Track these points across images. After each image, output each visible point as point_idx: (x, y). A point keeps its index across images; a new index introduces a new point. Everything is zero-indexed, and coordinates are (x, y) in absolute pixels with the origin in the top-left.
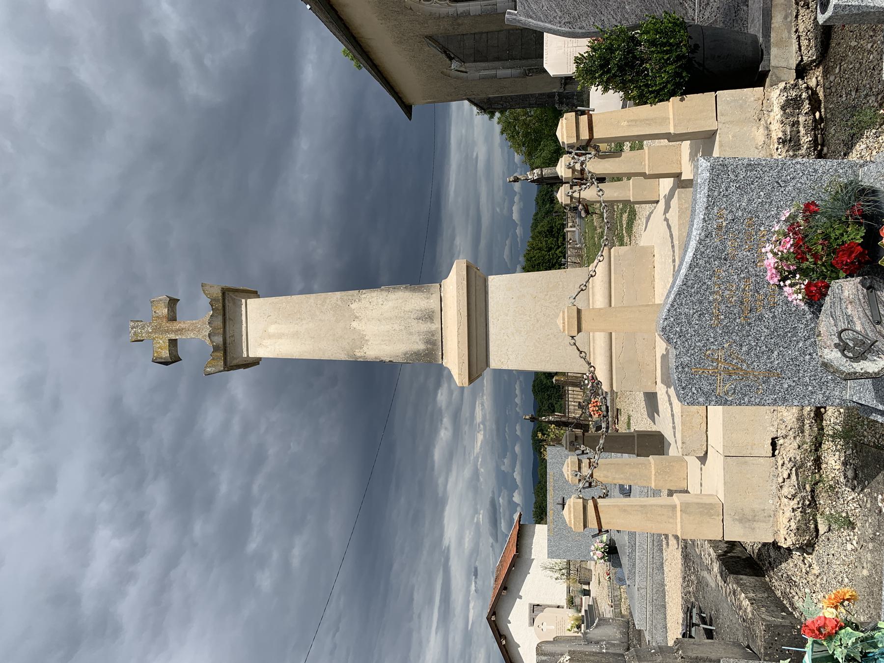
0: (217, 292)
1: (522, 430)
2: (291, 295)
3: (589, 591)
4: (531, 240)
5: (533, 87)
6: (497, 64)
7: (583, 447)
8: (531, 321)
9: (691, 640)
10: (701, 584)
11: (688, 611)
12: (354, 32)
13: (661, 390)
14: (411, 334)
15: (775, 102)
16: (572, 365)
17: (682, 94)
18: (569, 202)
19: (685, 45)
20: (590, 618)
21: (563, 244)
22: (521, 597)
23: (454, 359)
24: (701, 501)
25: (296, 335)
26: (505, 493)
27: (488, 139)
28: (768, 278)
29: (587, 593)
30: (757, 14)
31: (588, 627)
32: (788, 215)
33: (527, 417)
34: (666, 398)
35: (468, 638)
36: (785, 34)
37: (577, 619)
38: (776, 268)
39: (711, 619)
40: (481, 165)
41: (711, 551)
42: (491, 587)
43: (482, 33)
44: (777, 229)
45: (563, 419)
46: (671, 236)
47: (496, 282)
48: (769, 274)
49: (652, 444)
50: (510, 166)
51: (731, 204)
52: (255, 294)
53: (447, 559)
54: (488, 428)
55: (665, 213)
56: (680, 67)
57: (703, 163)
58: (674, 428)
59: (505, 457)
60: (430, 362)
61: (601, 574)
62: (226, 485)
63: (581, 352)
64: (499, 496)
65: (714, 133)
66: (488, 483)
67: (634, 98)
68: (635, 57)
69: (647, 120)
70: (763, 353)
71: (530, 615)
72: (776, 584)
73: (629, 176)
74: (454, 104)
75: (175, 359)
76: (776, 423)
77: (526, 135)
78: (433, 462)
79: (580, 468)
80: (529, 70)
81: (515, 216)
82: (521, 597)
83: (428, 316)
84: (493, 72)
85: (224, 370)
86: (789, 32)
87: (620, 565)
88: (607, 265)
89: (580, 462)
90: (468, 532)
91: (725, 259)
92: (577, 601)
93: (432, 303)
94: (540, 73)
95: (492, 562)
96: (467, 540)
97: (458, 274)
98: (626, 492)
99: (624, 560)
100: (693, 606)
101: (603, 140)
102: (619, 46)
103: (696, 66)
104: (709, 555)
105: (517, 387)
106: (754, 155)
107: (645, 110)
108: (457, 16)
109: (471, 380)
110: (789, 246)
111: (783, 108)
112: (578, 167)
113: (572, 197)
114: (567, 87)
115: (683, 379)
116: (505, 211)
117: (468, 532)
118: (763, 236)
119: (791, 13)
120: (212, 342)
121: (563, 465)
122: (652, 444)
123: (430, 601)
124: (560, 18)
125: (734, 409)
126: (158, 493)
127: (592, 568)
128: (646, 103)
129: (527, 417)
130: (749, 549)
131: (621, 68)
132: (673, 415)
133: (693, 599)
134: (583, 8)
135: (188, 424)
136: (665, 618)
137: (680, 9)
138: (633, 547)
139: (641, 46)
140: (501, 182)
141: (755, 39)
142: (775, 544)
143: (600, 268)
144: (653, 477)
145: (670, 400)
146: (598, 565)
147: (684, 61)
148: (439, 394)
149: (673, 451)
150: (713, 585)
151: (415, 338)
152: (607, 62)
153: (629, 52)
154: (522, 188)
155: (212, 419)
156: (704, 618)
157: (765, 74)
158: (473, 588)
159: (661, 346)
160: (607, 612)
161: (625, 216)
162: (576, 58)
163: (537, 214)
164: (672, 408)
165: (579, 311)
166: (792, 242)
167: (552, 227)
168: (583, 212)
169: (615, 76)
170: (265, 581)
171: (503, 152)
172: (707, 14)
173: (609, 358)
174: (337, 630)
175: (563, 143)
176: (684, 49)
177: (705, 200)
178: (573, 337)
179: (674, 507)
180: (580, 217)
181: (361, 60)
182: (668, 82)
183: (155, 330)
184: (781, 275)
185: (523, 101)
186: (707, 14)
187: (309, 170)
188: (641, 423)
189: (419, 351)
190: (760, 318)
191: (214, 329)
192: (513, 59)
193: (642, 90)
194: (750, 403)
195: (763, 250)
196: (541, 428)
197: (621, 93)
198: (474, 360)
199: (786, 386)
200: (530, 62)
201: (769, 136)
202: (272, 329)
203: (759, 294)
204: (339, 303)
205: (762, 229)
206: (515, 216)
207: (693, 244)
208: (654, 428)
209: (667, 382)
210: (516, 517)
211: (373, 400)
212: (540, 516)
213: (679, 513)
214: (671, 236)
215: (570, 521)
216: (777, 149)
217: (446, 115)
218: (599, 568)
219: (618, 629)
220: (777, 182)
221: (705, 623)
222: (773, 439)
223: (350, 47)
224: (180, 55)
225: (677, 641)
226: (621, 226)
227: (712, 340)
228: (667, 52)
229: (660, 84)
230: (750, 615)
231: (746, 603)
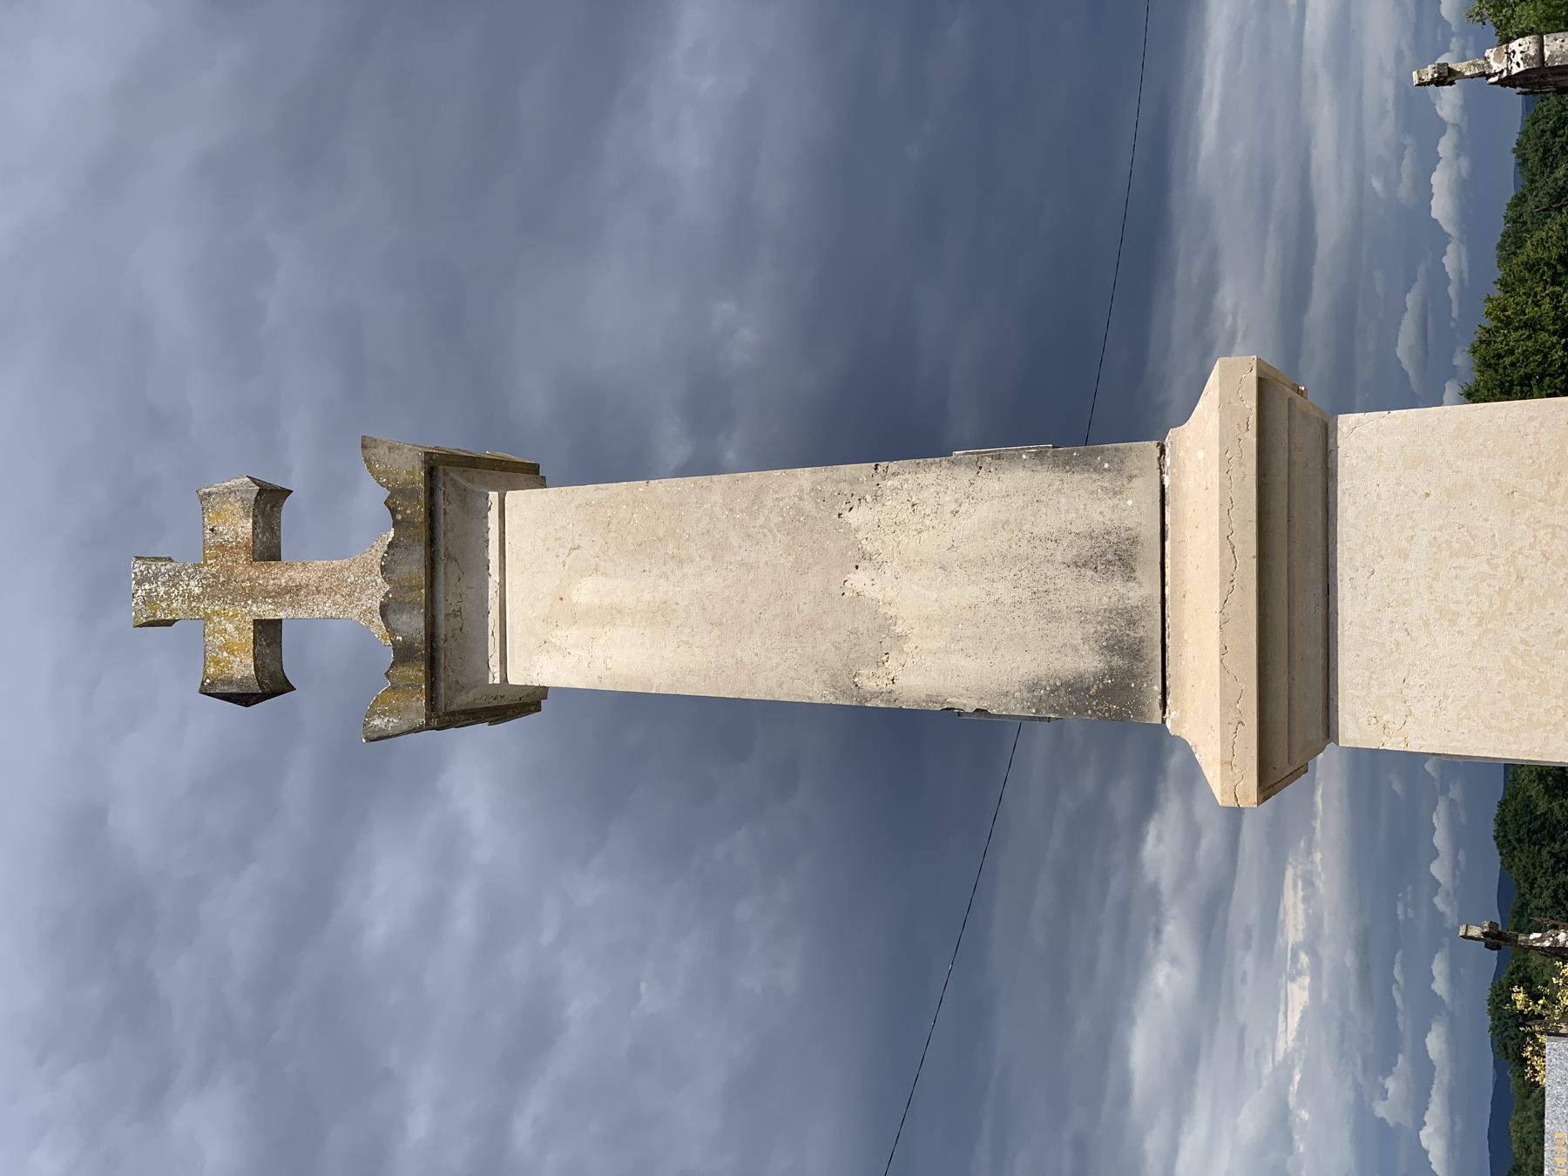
0: (410, 468)
1: (1453, 978)
4: (1497, 293)
14: (1054, 616)
25: (660, 614)
33: (1475, 931)
47: (1369, 442)
52: (530, 474)
54: (1326, 966)
59: (1387, 1070)
60: (1119, 717)
75: (270, 684)
81: (1441, 207)
83: (1115, 556)
85: (427, 727)
97: (1224, 405)
105: (1439, 820)
109: (1268, 784)
116: (1404, 190)
120: (392, 631)
129: (1475, 931)
140: (1389, 88)
148: (1151, 839)
151: (1072, 632)
155: (387, 888)
163: (1520, 200)
183: (214, 589)
191: (399, 587)
202: (585, 592)
204: (808, 505)
206: (1441, 207)
211: (928, 847)
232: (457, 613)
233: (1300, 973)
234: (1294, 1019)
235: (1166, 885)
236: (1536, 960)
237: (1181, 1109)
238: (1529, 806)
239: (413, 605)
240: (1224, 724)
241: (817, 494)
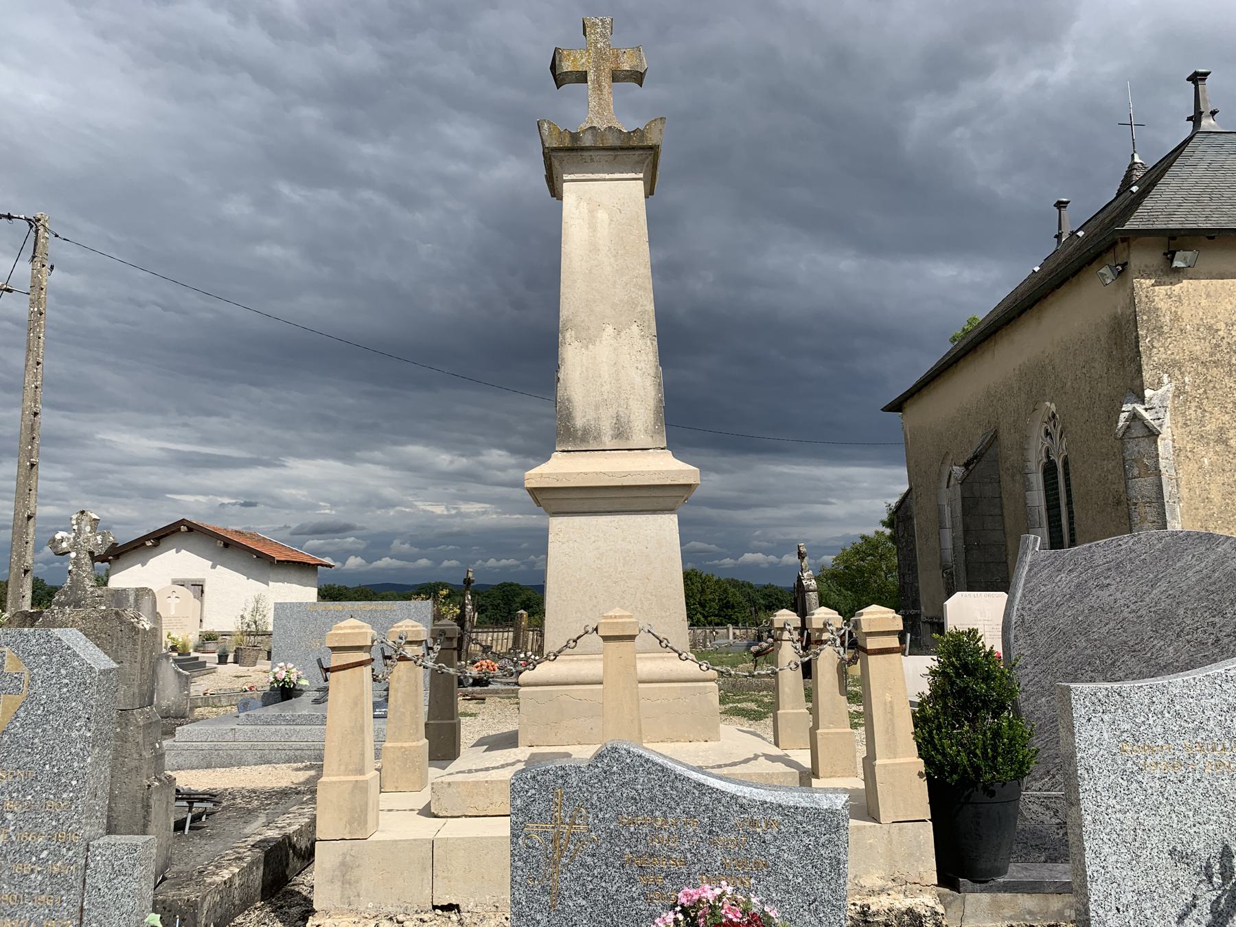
0: (653, 139)
1: (450, 568)
2: (650, 241)
3: (226, 663)
4: (715, 578)
5: (928, 580)
6: (960, 528)
7: (437, 648)
8: (614, 575)
9: (173, 798)
10: (250, 814)
11: (210, 797)
12: (1003, 332)
13: (521, 753)
14: (597, 408)
15: (917, 900)
16: (556, 627)
17: (928, 774)
18: (776, 625)
19: (993, 777)
20: (189, 664)
21: (710, 623)
22: (213, 567)
23: (562, 468)
24: (370, 809)
25: (594, 248)
26: (361, 545)
27: (854, 519)
28: (686, 889)
29: (223, 659)
30: (1035, 874)
31: (176, 661)
32: (772, 914)
33: (470, 575)
34: (510, 761)
35: (153, 493)
36: (1008, 912)
37: (184, 646)
38: (699, 901)
39: (199, 828)
40: (819, 509)
41: (296, 827)
42: (228, 525)
43: (1002, 508)
44: (754, 900)
45: (468, 625)
46: (734, 764)
47: (666, 526)
48: (691, 891)
49: (444, 746)
50: (823, 549)
51: (785, 839)
52: (650, 192)
53: (267, 464)
54: (451, 520)
55: (764, 755)
56: (965, 771)
57: (840, 801)
58: (470, 771)
59: (412, 544)
60: (558, 434)
61: (250, 679)
62: (372, 152)
63: (575, 641)
64: (357, 537)
65: (876, 820)
66: (376, 521)
67: (922, 710)
68: (977, 710)
69: (893, 728)
70: (583, 885)
71: (188, 580)
72: (253, 916)
73: (814, 712)
74: (904, 472)
75: (560, 79)
76: (479, 909)
77: (860, 571)
78: (403, 444)
79: (411, 643)
80: (951, 573)
81: (748, 557)
82: (213, 567)
83: (621, 431)
84: (948, 524)
85: (544, 148)
86: (1011, 918)
87: (265, 705)
88: (693, 677)
89: (419, 643)
90: (305, 492)
91: (710, 832)
92: (211, 646)
93: (640, 437)
94: (947, 589)
95: (264, 527)
96: (293, 491)
97: (681, 472)
98: (381, 703)
99: (273, 710)
100: (216, 803)
101: (865, 668)
102: (993, 689)
103: (966, 793)
104: (290, 825)
105: (512, 562)
106: (850, 869)
107: (906, 726)
108: (1025, 474)
109: (532, 491)
110: (730, 916)
111: (910, 911)
112: (825, 636)
113: (782, 629)
114: (928, 626)
115: (547, 777)
116: (756, 543)
117: (305, 492)
118: (742, 883)
119: (1036, 920)
120: (583, 132)
121: (412, 622)
122: (444, 746)
123: (207, 440)
124: (1030, 609)
125: (507, 847)
126: (361, 57)
127: (258, 667)
128: (916, 726)
129: (470, 575)
130: (299, 879)
131: (962, 692)
132: (487, 769)
133: (225, 804)
134: (1042, 640)
135: (457, 100)
136: (192, 768)
137: (1042, 771)
138: (292, 722)
139: (993, 718)
140: (795, 537)
141: (1001, 871)
142: (312, 912)
143: (691, 667)
144: (399, 744)
145: (508, 765)
146: (262, 675)
147: (973, 776)
148: (500, 452)
149: (434, 773)
150: (248, 830)
151: (591, 415)
152: (970, 673)
153: (984, 702)
154: (788, 567)
155: (465, 133)
156: (200, 819)
157: (955, 887)
158: (226, 500)
159: (583, 753)
160: (198, 688)
161: (753, 706)
162: (976, 631)
163: (751, 586)
164: (497, 768)
165: (632, 638)
166: (735, 920)
167: (733, 607)
168: (757, 648)
169: (953, 683)
170: (237, 208)
171: (837, 539)
172: (1034, 807)
173: (565, 681)
174: (165, 309)
175: (862, 614)
176: (988, 776)
177: (791, 803)
178: (596, 629)
179: (361, 772)
180: (749, 646)
181: (965, 342)
182: (944, 755)
183: (599, 53)
184: (691, 907)
185: (908, 566)
186: (1034, 807)
187: (816, 272)
188: (470, 731)
189: (573, 419)
190: (631, 881)
191: (603, 134)
192: (967, 550)
193: (929, 725)
194: (514, 868)
195: (724, 883)
196: (455, 595)
197: (928, 693)
199: (538, 917)
200: (963, 574)
201: (872, 893)
202: (602, 215)
203: (664, 878)
204: (639, 309)
205: (752, 881)
206: (748, 557)
207: (731, 788)
208: (463, 749)
209: (533, 760)
210: (327, 560)
211: (500, 358)
212: (328, 594)
213: (353, 778)
214: (734, 764)
215: (341, 628)
216: (854, 904)
217: (888, 461)
218: (260, 675)
219: (174, 703)
220: (815, 900)
221: (192, 821)
222: (457, 906)
223: (982, 327)
224: (969, 94)
225: (171, 780)
226: (739, 701)
227: (600, 816)
228: (985, 753)
229: (942, 745)
230: (209, 880)
231: (226, 874)
232: (592, 160)
233: (448, 510)
234: (430, 508)
235: (482, 458)
236: (458, 599)
237: (392, 466)
238: (519, 594)
239: (595, 141)
240: (556, 474)
241: (644, 312)
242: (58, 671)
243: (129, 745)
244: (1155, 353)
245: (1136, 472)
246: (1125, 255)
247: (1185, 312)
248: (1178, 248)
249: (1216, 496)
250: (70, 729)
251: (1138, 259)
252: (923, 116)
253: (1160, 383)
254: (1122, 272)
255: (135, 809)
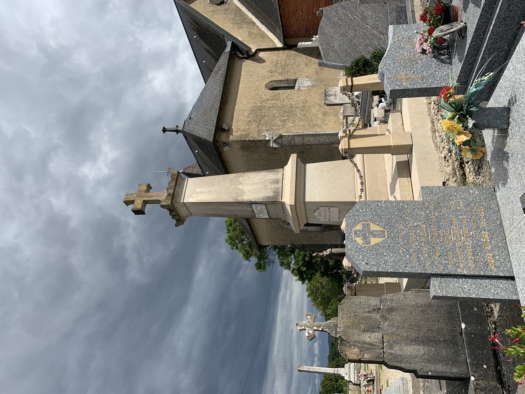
25: (210, 192)
83: (276, 182)
151: (269, 191)
190: (417, 63)
191: (170, 186)
198: (298, 200)
202: (198, 190)
241: (235, 177)
242: (361, 212)
243: (394, 299)
244: (254, 136)
245: (293, 142)
246: (221, 143)
247: (242, 128)
248: (221, 128)
249: (302, 123)
250: (382, 207)
251: (223, 138)
252: (135, 274)
253: (264, 135)
254: (226, 144)
255: (420, 296)
